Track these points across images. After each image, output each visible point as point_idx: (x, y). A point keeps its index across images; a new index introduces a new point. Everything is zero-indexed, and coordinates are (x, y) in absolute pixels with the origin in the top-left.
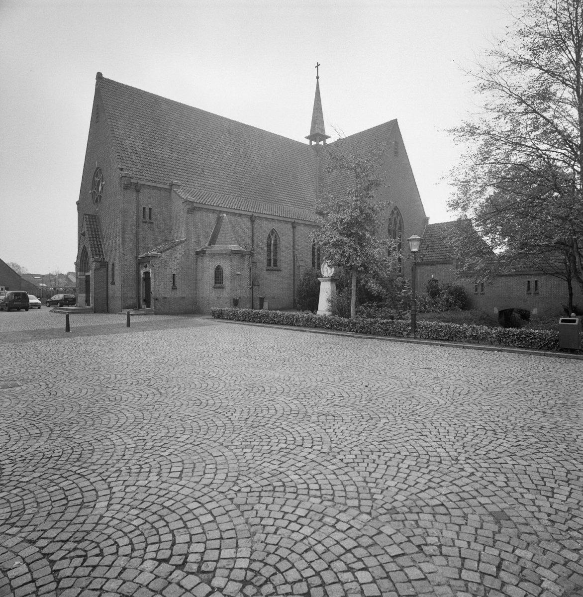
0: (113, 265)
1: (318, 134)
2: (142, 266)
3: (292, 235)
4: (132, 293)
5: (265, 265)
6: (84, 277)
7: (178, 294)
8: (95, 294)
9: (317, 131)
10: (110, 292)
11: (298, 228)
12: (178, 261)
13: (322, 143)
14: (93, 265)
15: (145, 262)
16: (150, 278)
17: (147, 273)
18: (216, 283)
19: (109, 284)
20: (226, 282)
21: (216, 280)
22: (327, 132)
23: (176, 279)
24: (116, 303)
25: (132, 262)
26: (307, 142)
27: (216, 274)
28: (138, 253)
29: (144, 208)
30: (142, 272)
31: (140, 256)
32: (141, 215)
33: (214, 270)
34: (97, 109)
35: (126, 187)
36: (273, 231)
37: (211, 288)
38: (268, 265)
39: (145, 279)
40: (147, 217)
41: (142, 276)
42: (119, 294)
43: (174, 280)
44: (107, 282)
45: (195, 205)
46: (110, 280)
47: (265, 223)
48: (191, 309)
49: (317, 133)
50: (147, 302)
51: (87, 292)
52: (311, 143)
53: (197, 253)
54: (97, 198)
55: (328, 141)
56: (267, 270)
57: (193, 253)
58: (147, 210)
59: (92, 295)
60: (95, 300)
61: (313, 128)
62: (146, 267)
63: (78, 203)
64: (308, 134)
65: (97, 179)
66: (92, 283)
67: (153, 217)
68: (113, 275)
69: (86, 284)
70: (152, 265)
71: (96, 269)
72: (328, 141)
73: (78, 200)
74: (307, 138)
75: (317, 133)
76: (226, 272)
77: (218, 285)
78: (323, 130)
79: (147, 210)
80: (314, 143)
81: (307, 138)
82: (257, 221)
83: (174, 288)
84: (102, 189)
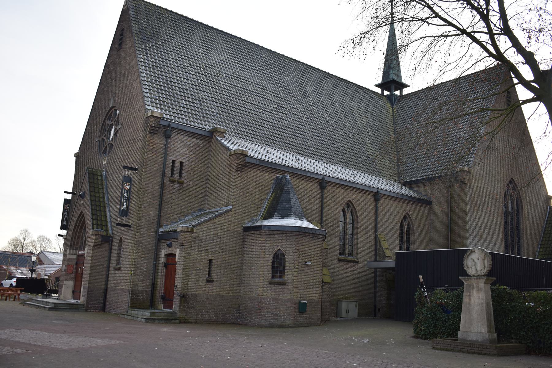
0: (121, 241)
1: (393, 81)
2: (164, 245)
3: (373, 212)
4: (144, 286)
5: (337, 252)
6: (75, 257)
7: (213, 290)
8: (89, 282)
9: (392, 76)
10: (112, 283)
11: (382, 201)
12: (218, 240)
13: (397, 93)
14: (91, 240)
15: (169, 239)
16: (175, 264)
17: (171, 256)
18: (273, 277)
19: (111, 269)
20: (289, 276)
21: (273, 272)
22: (405, 79)
23: (214, 267)
24: (120, 299)
25: (149, 241)
26: (379, 90)
27: (274, 263)
28: (160, 226)
29: (174, 162)
30: (163, 253)
31: (161, 230)
32: (168, 172)
33: (272, 257)
34: (122, 35)
35: (153, 131)
36: (349, 204)
37: (266, 283)
38: (340, 254)
39: (166, 265)
40: (176, 176)
41: (162, 259)
42: (125, 286)
43: (210, 268)
44: (109, 266)
45: (247, 160)
46: (113, 264)
47: (339, 192)
48: (234, 316)
49: (391, 80)
50: (167, 300)
51: (78, 279)
52: (383, 93)
53: (247, 229)
54: (106, 147)
55: (406, 91)
56: (339, 260)
57: (240, 230)
58: (177, 165)
59: (85, 283)
60: (90, 292)
61: (386, 74)
62: (169, 246)
63: (77, 156)
64: (380, 81)
65: (109, 123)
66: (87, 268)
67: (185, 174)
68: (119, 256)
69: (73, 267)
70: (182, 245)
71: (96, 246)
72: (406, 91)
73: (77, 150)
74: (378, 86)
75: (391, 80)
76: (290, 259)
77: (277, 280)
78: (400, 77)
79: (177, 165)
80: (386, 93)
81: (378, 86)
82: (329, 188)
83: (210, 281)
84: (116, 134)
